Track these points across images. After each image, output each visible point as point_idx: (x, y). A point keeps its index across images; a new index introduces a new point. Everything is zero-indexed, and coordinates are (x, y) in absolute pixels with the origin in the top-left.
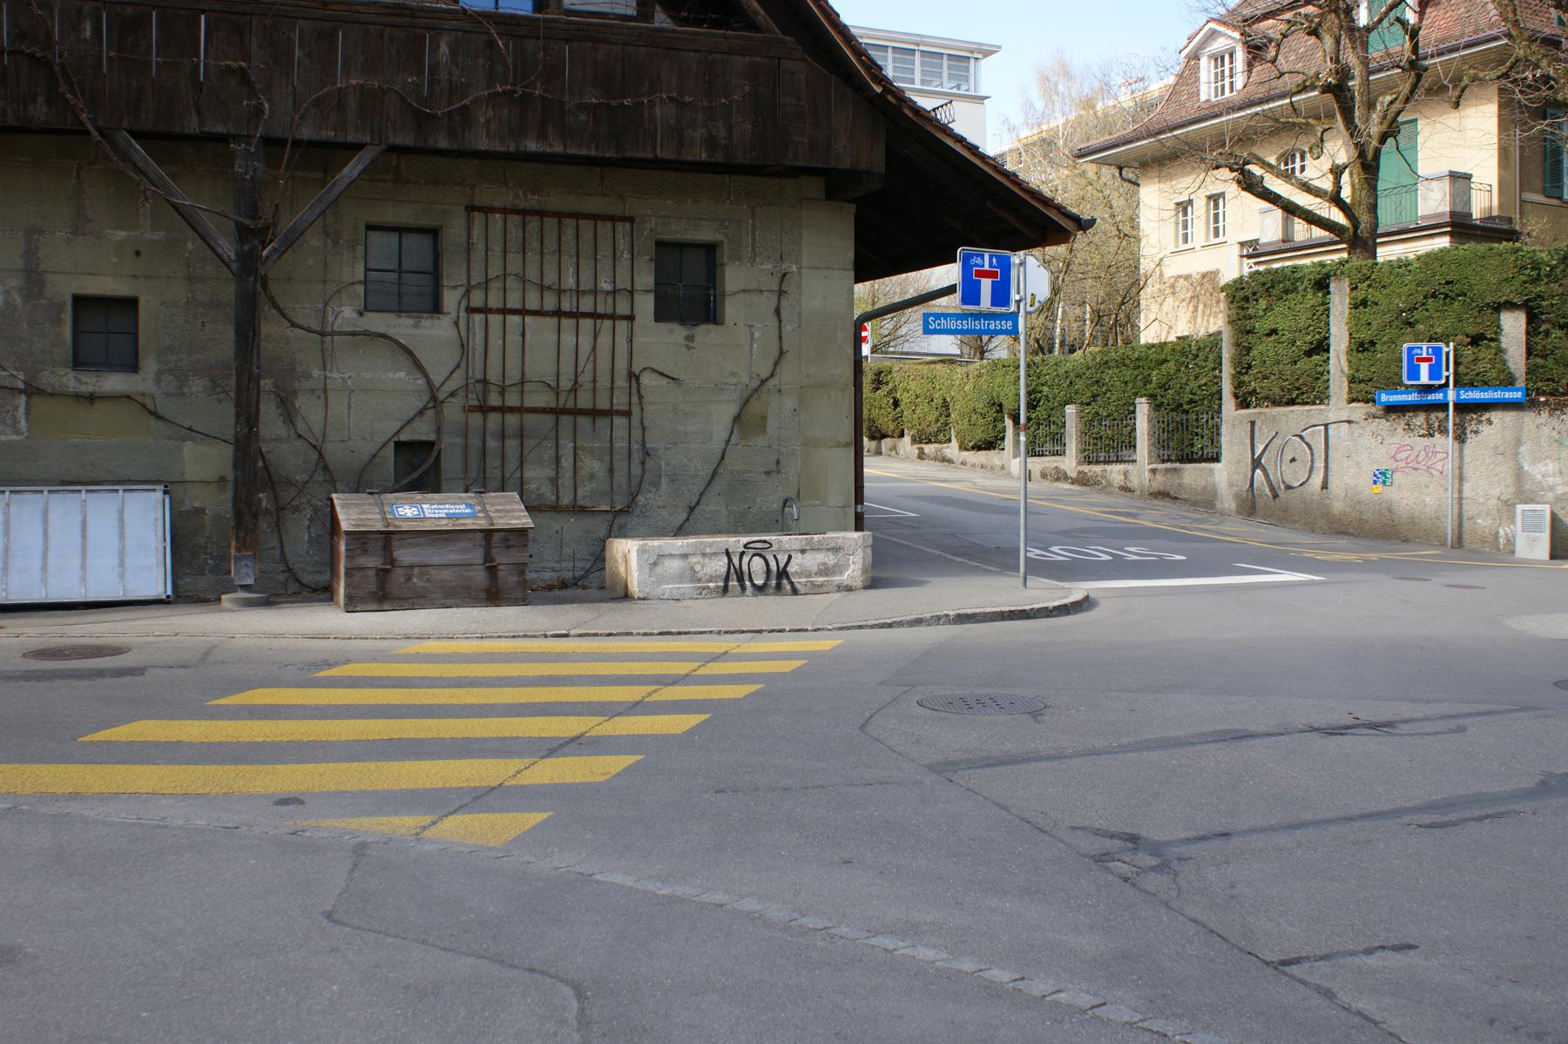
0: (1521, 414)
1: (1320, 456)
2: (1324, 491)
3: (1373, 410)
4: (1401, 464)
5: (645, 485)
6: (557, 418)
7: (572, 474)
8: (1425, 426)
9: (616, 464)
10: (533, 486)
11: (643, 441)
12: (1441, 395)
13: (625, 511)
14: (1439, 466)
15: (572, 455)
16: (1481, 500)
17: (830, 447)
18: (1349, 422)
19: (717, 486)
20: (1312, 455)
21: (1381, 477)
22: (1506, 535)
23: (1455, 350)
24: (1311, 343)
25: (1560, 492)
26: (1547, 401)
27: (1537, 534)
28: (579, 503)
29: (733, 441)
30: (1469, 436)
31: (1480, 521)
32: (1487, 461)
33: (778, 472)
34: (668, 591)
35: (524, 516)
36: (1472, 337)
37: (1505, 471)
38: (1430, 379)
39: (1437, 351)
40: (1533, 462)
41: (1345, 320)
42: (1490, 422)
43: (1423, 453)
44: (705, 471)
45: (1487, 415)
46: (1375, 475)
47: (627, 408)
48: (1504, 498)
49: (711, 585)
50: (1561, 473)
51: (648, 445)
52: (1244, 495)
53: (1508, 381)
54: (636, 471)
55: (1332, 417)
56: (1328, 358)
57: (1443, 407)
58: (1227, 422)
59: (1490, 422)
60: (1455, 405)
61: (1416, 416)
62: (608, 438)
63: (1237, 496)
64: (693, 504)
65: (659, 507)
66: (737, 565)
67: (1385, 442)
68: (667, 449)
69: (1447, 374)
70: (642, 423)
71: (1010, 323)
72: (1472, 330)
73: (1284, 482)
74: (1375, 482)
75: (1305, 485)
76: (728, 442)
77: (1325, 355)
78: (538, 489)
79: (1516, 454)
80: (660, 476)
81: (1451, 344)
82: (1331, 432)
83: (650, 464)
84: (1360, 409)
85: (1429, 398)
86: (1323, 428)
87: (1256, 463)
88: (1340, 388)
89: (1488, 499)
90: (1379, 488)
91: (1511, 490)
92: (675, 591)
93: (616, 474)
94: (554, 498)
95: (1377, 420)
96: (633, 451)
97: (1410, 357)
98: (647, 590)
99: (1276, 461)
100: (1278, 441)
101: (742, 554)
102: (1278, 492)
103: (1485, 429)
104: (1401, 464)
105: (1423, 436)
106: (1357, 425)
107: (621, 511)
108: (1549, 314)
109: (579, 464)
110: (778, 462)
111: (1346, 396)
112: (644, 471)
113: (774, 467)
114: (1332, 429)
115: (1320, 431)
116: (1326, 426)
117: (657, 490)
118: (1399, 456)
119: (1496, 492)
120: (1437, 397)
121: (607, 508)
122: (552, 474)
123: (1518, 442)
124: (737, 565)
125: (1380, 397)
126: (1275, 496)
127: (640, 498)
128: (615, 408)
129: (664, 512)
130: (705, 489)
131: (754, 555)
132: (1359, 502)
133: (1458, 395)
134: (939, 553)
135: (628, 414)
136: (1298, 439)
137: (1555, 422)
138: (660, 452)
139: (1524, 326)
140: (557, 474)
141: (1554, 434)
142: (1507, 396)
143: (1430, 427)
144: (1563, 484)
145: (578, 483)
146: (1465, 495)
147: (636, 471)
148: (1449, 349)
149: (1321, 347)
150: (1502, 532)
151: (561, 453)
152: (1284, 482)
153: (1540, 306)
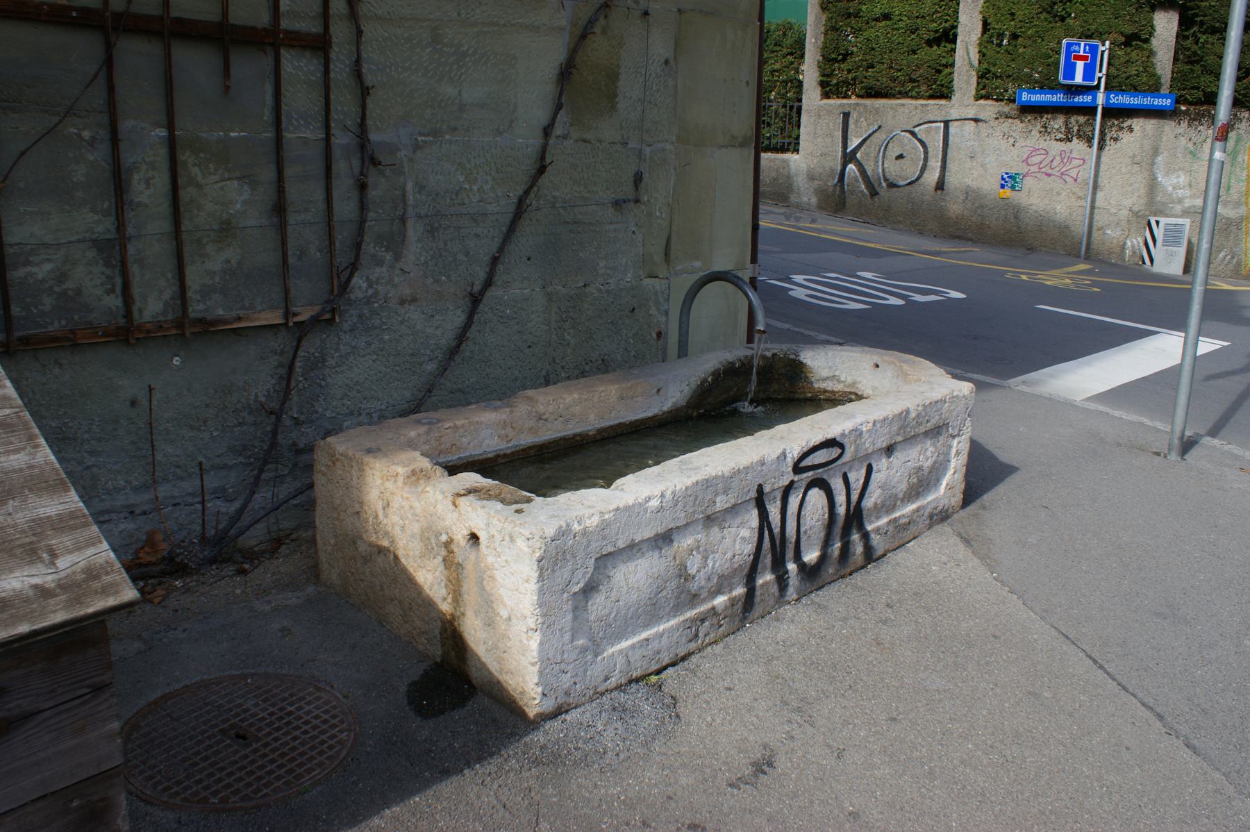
0: (1162, 122)
1: (936, 156)
2: (939, 192)
3: (1006, 109)
4: (1033, 169)
5: (369, 247)
6: (109, 47)
7: (165, 225)
8: (1063, 130)
9: (292, 192)
10: (43, 270)
11: (362, 124)
12: (1090, 97)
13: (326, 320)
14: (1073, 173)
15: (164, 166)
16: (1113, 211)
17: (720, 147)
18: (976, 120)
19: (526, 240)
20: (926, 152)
21: (1010, 180)
22: (1133, 246)
23: (1110, 49)
24: (936, 31)
25: (1187, 205)
26: (1188, 110)
27: (1175, 249)
28: (196, 309)
29: (558, 131)
30: (1108, 142)
31: (1109, 232)
32: (1124, 170)
33: (637, 201)
34: (620, 662)
35: (63, 524)
36: (1126, 37)
37: (1139, 182)
38: (1083, 80)
39: (1094, 49)
40: (1167, 174)
41: (979, 8)
42: (1131, 129)
43: (1058, 158)
44: (500, 206)
45: (1128, 122)
46: (1003, 179)
47: (315, 28)
48: (1136, 209)
49: (720, 600)
50: (1190, 185)
51: (374, 136)
52: (831, 190)
53: (1154, 89)
54: (345, 208)
55: (954, 114)
56: (954, 50)
57: (1090, 111)
58: (809, 112)
59: (1131, 129)
60: (1104, 109)
61: (1054, 119)
62: (267, 115)
63: (820, 192)
64: (477, 288)
65: (402, 302)
66: (777, 530)
67: (1017, 145)
68: (417, 147)
69: (1100, 75)
70: (358, 75)
71: (1090, 97)
72: (1128, 29)
73: (886, 180)
74: (1002, 187)
75: (915, 185)
76: (547, 131)
77: (949, 46)
78: (62, 277)
79: (1153, 164)
80: (403, 220)
81: (1107, 43)
82: (952, 130)
83: (379, 188)
84: (989, 109)
85: (1076, 100)
86: (942, 124)
87: (849, 157)
88: (968, 82)
89: (1120, 210)
90: (1007, 192)
91: (1143, 201)
92: (635, 656)
93: (292, 218)
94: (115, 302)
95: (1010, 120)
96: (337, 152)
97: (1068, 53)
98: (566, 680)
99: (877, 157)
100: (881, 137)
101: (787, 491)
102: (878, 189)
103: (1125, 137)
104: (1033, 169)
105: (1060, 140)
106: (984, 125)
107: (315, 320)
108: (1205, 16)
109: (186, 194)
110: (638, 179)
111: (974, 92)
112: (363, 207)
113: (628, 190)
114: (953, 128)
115: (939, 128)
116: (946, 123)
117: (397, 257)
118: (1031, 161)
119: (1128, 202)
120: (1086, 99)
121: (275, 318)
122: (105, 227)
123: (1156, 152)
124: (777, 530)
125: (1020, 96)
126: (874, 193)
127: (358, 281)
128: (285, 24)
129: (414, 314)
130: (501, 250)
131: (809, 487)
132: (982, 206)
133: (1108, 98)
134: (787, 326)
135: (319, 45)
136: (907, 135)
137: (1192, 133)
138: (402, 154)
139: (1176, 28)
140: (121, 226)
141: (1190, 145)
142: (1156, 103)
143: (1068, 130)
144: (1191, 197)
145: (187, 249)
146: (1097, 204)
147: (345, 208)
148: (1104, 47)
149: (948, 37)
150: (1129, 243)
151: (128, 159)
152: (886, 180)
153: (1198, 7)
